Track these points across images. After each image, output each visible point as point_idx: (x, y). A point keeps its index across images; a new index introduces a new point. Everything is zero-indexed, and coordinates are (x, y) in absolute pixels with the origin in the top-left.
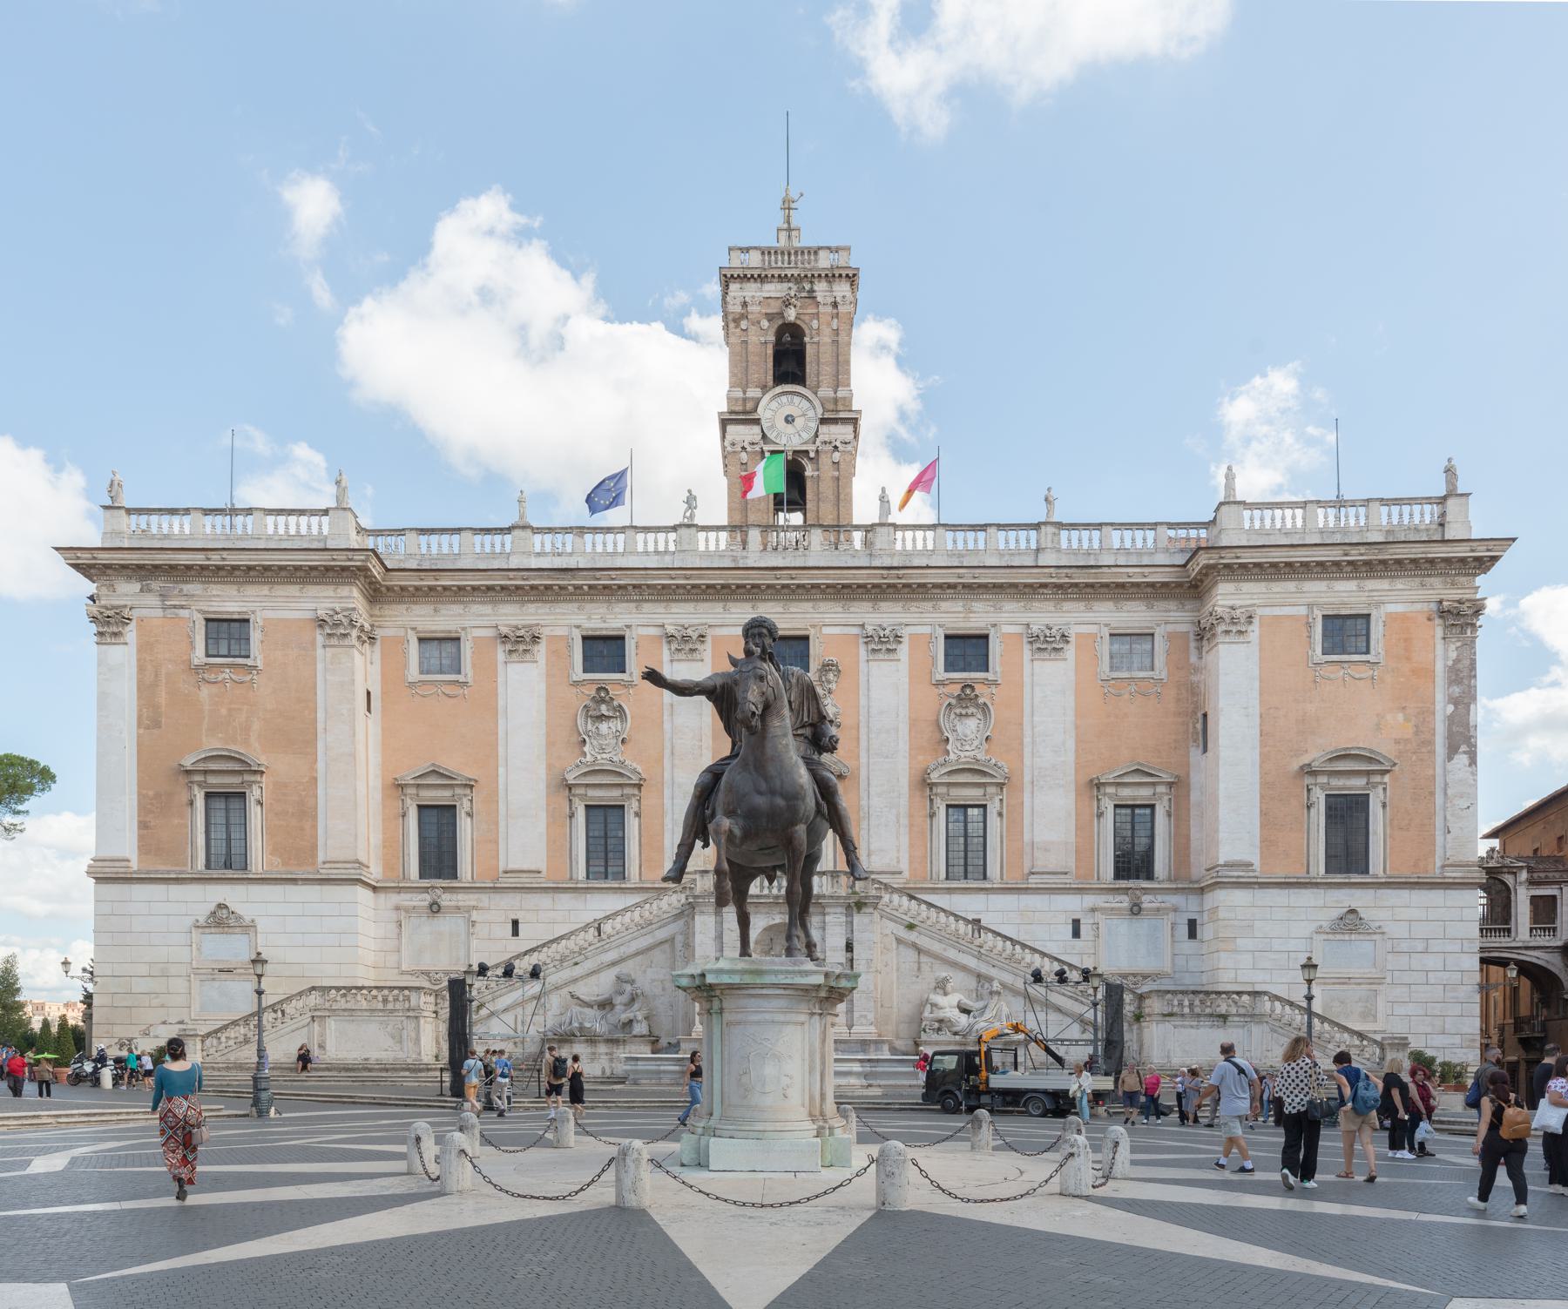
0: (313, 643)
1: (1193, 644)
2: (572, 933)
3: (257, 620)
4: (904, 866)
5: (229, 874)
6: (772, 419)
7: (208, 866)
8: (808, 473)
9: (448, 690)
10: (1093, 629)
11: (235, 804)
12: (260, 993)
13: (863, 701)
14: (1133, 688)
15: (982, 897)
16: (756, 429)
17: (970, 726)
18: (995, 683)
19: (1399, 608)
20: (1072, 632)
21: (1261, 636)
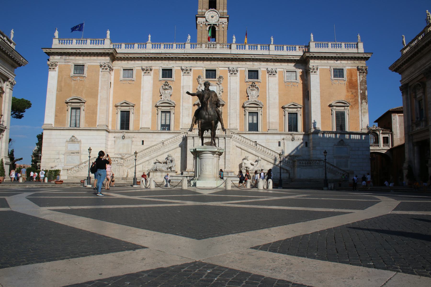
0: (99, 71)
2: (157, 144)
3: (86, 65)
4: (238, 127)
5: (76, 128)
7: (70, 126)
8: (216, 29)
9: (130, 82)
11: (78, 111)
12: (90, 157)
13: (229, 86)
15: (257, 136)
16: (204, 19)
17: (254, 93)
18: (260, 82)
19: (350, 68)
20: (278, 70)
21: (320, 73)
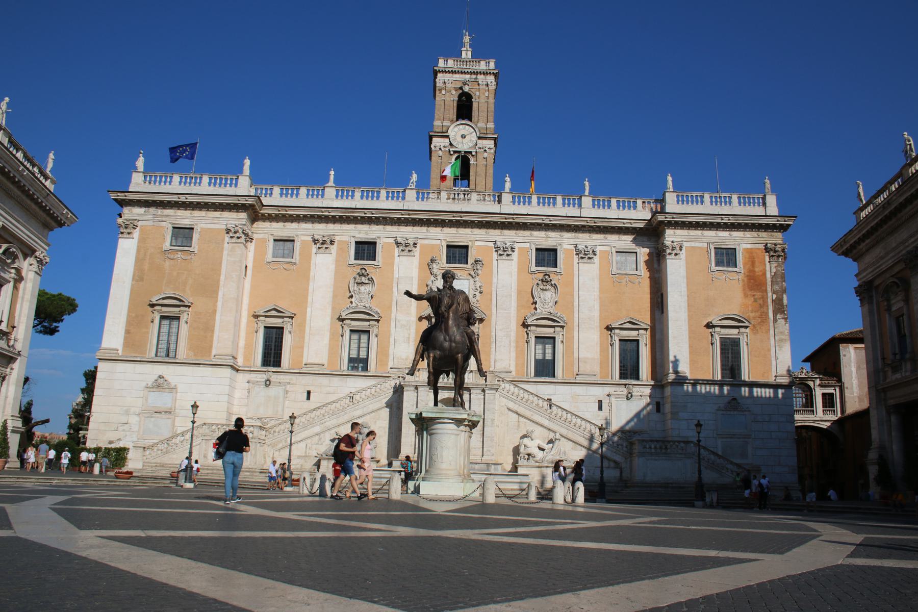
0: (223, 240)
1: (655, 259)
2: (339, 400)
3: (197, 229)
4: (513, 368)
5: (167, 360)
6: (455, 136)
7: (156, 355)
9: (286, 266)
10: (608, 249)
11: (175, 323)
12: (193, 422)
13: (494, 280)
14: (627, 279)
15: (552, 386)
16: (447, 140)
18: (560, 273)
